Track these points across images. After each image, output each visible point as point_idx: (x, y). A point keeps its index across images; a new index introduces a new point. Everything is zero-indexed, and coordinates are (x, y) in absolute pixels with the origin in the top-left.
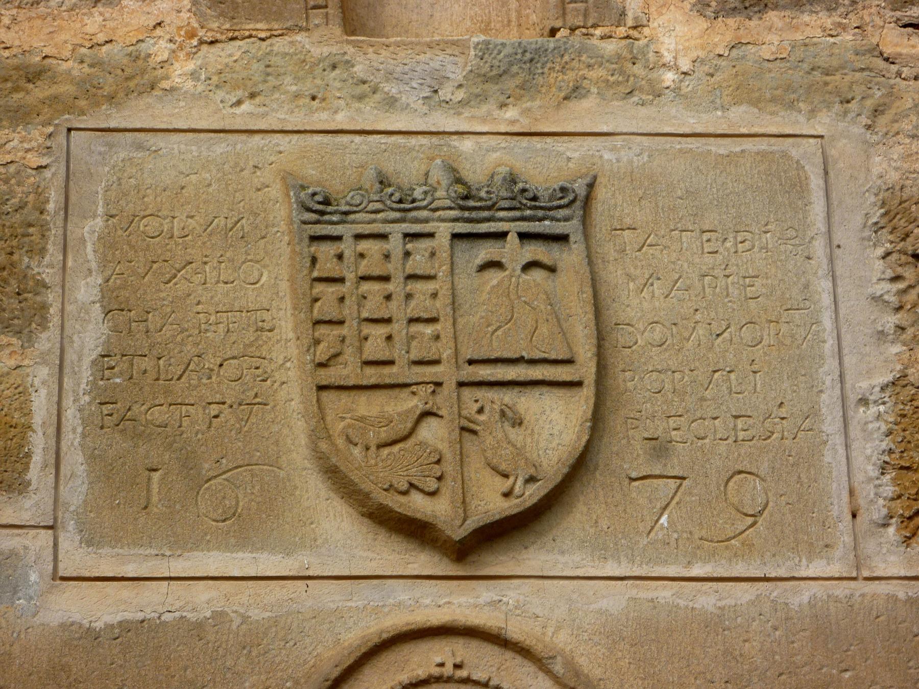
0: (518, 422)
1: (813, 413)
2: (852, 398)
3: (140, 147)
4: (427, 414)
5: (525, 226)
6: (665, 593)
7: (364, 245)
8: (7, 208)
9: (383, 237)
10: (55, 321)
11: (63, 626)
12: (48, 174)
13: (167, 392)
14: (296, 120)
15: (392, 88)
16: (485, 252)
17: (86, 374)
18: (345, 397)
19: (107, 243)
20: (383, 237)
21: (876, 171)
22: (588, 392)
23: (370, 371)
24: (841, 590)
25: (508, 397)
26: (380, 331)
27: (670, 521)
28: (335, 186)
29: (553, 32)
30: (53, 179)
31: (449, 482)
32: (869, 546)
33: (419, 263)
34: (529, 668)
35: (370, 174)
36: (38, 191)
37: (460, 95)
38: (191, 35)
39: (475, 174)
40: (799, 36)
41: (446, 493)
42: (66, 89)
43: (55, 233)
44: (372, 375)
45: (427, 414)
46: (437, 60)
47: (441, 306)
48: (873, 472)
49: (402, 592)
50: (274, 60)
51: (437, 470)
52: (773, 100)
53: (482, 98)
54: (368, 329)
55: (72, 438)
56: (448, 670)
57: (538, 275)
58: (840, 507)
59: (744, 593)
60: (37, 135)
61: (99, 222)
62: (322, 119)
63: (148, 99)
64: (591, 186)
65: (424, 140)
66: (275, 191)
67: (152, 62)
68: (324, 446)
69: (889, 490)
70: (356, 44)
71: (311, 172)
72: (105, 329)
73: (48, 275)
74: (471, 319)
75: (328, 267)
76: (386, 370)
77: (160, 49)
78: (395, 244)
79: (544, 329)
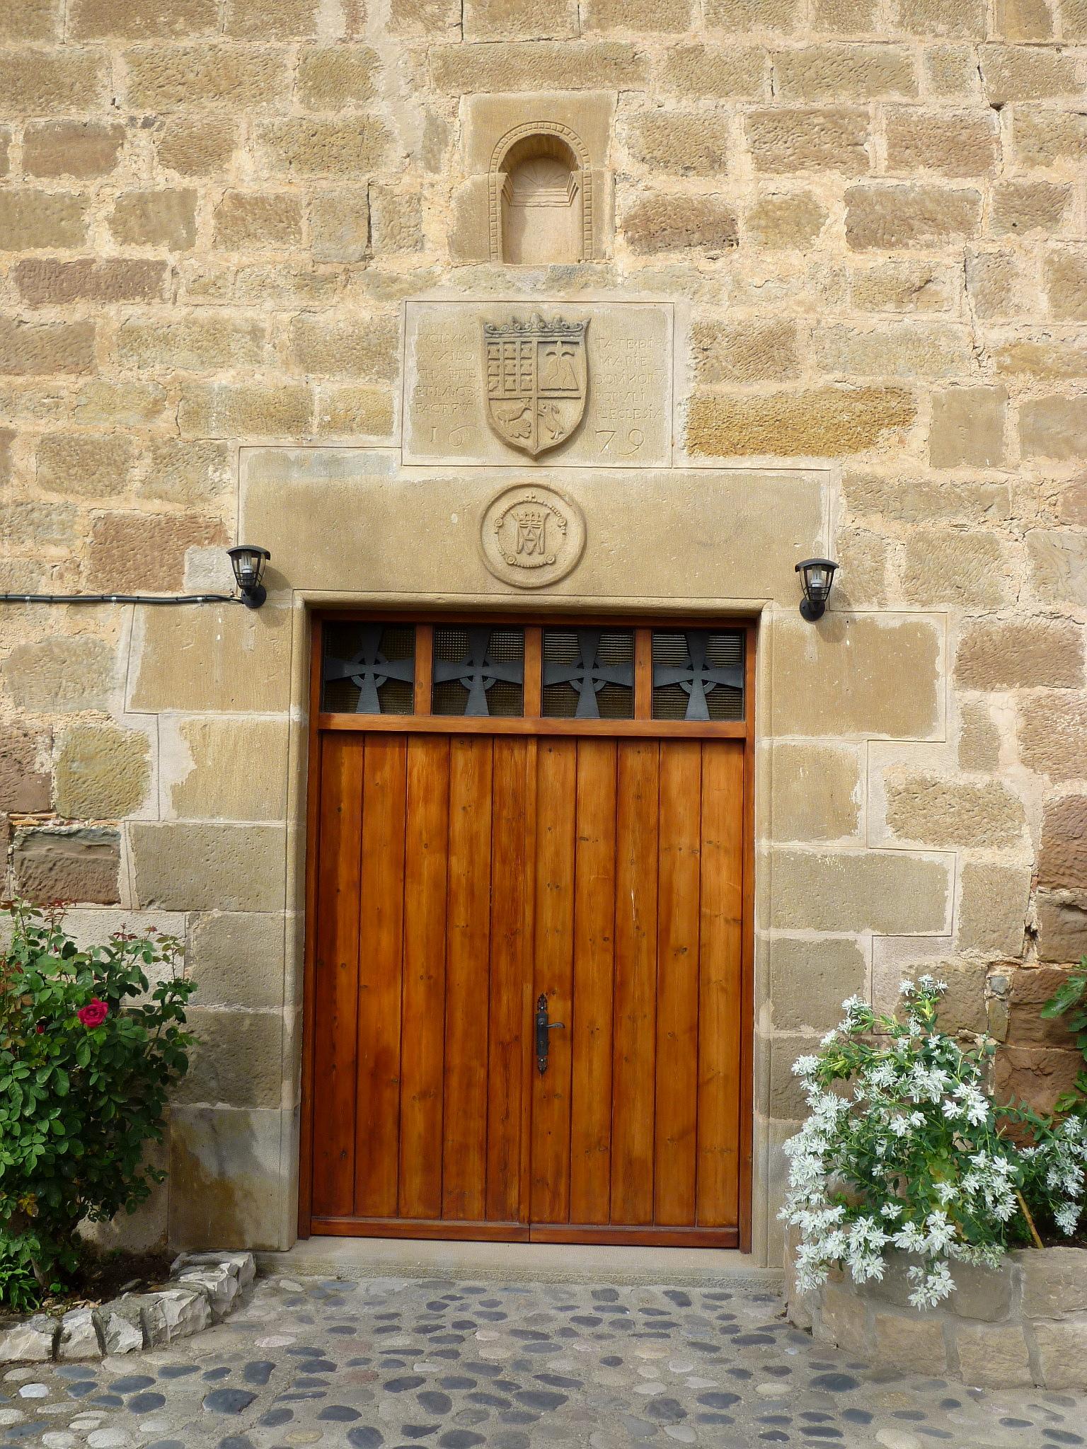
0: (558, 412)
1: (662, 408)
2: (676, 403)
3: (431, 308)
4: (526, 409)
5: (564, 339)
6: (605, 472)
7: (507, 346)
8: (2, 645)
9: (514, 343)
10: (401, 374)
11: (405, 482)
12: (399, 318)
13: (439, 400)
14: (485, 298)
15: (519, 284)
16: (550, 348)
17: (412, 393)
18: (498, 402)
19: (419, 345)
20: (514, 343)
21: (692, 316)
22: (582, 401)
23: (507, 393)
24: (665, 472)
25: (555, 402)
26: (512, 378)
27: (609, 448)
28: (498, 322)
29: (579, 261)
30: (401, 319)
31: (532, 433)
32: (677, 456)
33: (525, 353)
34: (557, 498)
35: (510, 318)
36: (395, 325)
37: (544, 287)
38: (449, 264)
39: (547, 318)
40: (669, 263)
41: (531, 438)
42: (405, 286)
43: (401, 341)
44: (508, 395)
45: (526, 409)
46: (536, 273)
47: (533, 368)
48: (680, 430)
49: (516, 472)
50: (479, 274)
51: (529, 429)
52: (657, 288)
53: (552, 288)
54: (507, 378)
55: (407, 416)
56: (530, 499)
57: (567, 357)
58: (668, 443)
59: (632, 473)
60: (395, 303)
61: (416, 337)
62: (494, 297)
63: (434, 289)
64: (589, 323)
65: (530, 304)
66: (477, 325)
67: (436, 274)
68: (491, 420)
69: (686, 437)
70: (507, 267)
71: (490, 317)
72: (418, 377)
73: (399, 356)
74: (543, 374)
75: (494, 355)
76: (513, 393)
77: (438, 269)
78: (517, 346)
79: (568, 378)
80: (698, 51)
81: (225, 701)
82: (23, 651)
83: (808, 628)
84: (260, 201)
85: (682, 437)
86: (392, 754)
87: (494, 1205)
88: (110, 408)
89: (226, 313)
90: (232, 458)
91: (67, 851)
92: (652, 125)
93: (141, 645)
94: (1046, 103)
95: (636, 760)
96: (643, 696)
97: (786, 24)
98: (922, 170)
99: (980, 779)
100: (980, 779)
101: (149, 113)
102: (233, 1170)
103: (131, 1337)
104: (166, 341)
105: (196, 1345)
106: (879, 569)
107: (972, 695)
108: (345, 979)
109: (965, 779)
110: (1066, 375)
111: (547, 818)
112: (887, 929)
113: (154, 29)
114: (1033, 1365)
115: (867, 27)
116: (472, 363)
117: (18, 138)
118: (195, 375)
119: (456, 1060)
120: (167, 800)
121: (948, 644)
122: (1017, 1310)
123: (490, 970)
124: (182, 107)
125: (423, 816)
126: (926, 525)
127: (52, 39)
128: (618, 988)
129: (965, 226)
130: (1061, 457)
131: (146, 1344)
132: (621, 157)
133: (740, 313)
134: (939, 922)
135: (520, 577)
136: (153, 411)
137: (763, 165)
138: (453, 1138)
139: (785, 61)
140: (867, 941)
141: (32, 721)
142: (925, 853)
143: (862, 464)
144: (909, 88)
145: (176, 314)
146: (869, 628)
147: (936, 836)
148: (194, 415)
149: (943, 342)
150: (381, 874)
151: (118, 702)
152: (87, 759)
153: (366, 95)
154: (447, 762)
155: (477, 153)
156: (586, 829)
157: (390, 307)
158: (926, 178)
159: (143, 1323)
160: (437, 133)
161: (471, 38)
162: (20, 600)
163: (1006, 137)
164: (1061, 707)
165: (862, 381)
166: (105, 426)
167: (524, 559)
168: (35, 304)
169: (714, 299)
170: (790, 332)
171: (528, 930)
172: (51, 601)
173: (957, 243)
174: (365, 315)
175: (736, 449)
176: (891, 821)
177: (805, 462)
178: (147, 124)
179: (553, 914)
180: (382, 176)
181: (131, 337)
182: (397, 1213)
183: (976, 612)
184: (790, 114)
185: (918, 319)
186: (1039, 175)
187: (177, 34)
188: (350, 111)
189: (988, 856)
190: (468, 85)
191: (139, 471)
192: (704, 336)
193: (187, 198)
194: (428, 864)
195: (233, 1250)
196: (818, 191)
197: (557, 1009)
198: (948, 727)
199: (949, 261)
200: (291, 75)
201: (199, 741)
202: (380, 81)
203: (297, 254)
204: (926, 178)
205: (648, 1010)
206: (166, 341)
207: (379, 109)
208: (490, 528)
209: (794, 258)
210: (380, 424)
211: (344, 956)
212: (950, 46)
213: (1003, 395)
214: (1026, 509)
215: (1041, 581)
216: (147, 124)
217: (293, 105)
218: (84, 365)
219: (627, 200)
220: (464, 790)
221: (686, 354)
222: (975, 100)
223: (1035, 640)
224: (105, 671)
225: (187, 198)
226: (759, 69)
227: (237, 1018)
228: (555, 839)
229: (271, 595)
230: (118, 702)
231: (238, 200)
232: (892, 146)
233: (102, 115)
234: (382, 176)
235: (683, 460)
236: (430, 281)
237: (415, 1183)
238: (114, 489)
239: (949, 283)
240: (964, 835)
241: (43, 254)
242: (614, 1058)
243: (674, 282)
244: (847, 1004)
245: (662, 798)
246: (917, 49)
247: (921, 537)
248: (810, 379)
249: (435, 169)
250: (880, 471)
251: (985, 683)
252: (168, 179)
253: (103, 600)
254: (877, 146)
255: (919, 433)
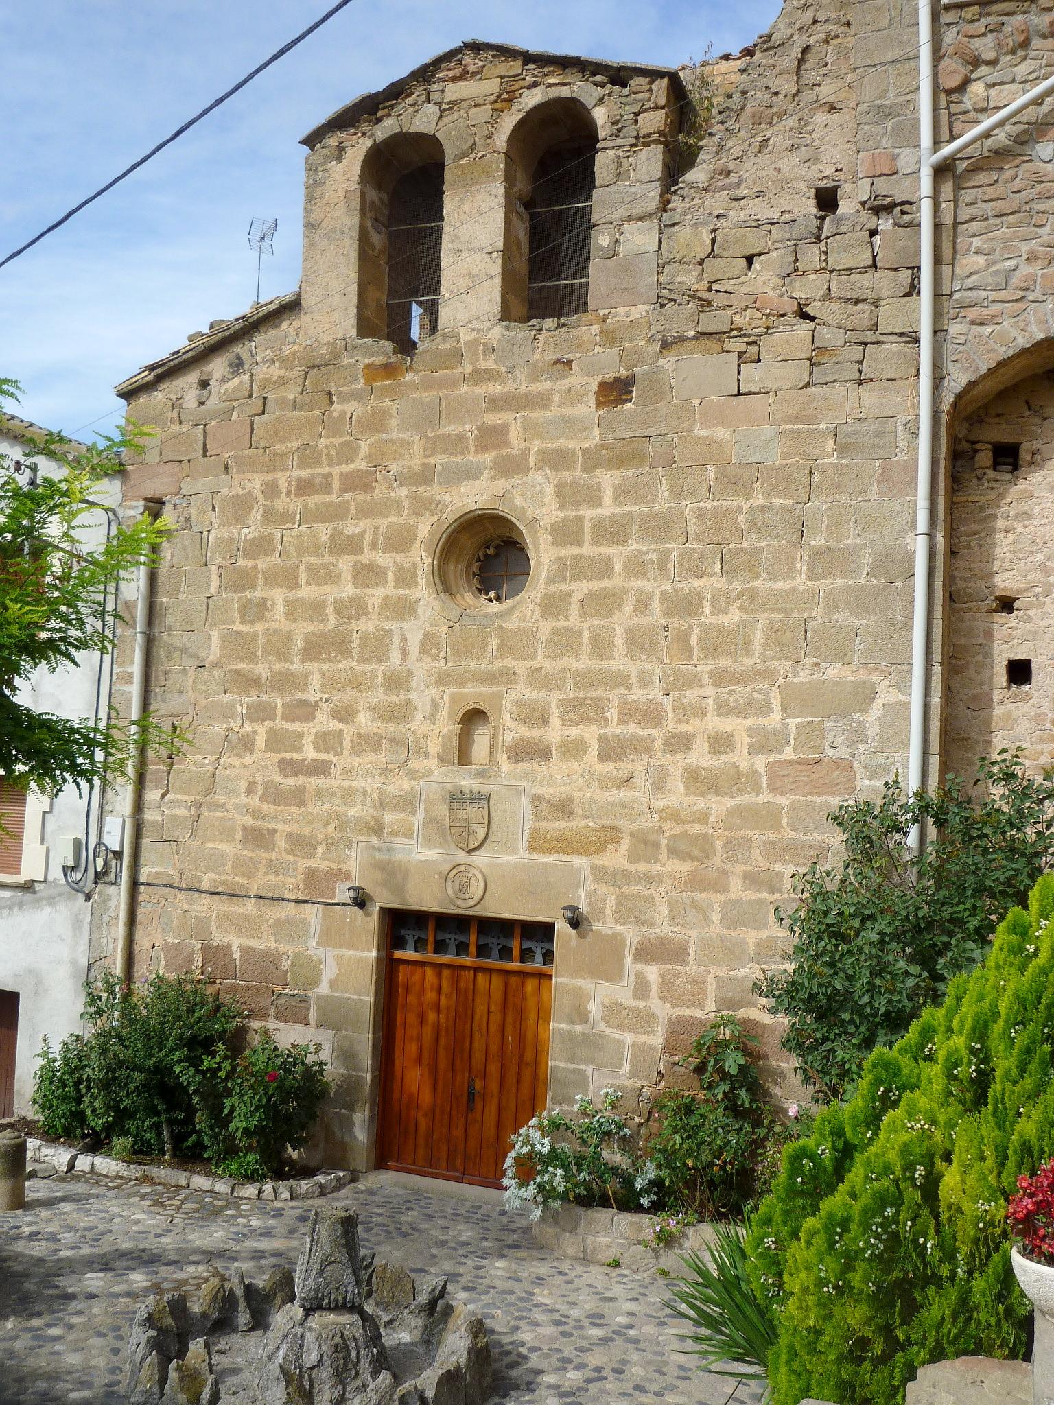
80: (540, 669)
81: (350, 947)
82: (278, 920)
83: (573, 932)
84: (367, 736)
85: (526, 845)
86: (419, 969)
87: (451, 1166)
88: (311, 822)
89: (354, 783)
90: (354, 846)
91: (292, 1002)
92: (520, 703)
93: (320, 921)
94: (688, 693)
95: (513, 980)
96: (516, 953)
97: (577, 656)
98: (632, 725)
99: (641, 1004)
100: (641, 1004)
101: (327, 696)
102: (346, 1138)
103: (286, 1195)
104: (332, 794)
105: (310, 1202)
106: (603, 908)
107: (640, 966)
108: (398, 1062)
109: (634, 1003)
110: (689, 822)
111: (478, 1001)
112: (599, 1066)
113: (329, 659)
114: (584, 1251)
115: (611, 658)
116: (443, 812)
117: (280, 706)
118: (342, 810)
119: (439, 1102)
120: (328, 985)
121: (631, 943)
122: (581, 1230)
123: (453, 1065)
124: (339, 694)
125: (430, 996)
126: (624, 889)
127: (292, 663)
128: (503, 1077)
129: (649, 751)
130: (684, 860)
131: (292, 1198)
132: (507, 719)
133: (552, 791)
134: (620, 1066)
135: (460, 903)
136: (326, 824)
137: (565, 723)
138: (436, 1135)
139: (576, 674)
140: (590, 1070)
141: (281, 949)
142: (617, 1035)
143: (599, 860)
144: (629, 687)
145: (336, 783)
146: (599, 933)
147: (622, 1027)
148: (341, 827)
149: (635, 806)
150: (412, 1018)
151: (312, 943)
152: (300, 966)
153: (408, 689)
154: (439, 975)
155: (450, 717)
156: (493, 1008)
157: (415, 784)
158: (634, 729)
159: (291, 1191)
160: (435, 706)
161: (450, 664)
162: (277, 899)
163: (669, 710)
164: (677, 974)
165: (601, 823)
166: (309, 829)
167: (461, 895)
168: (285, 777)
169: (541, 784)
170: (572, 800)
171: (467, 1050)
172: (288, 900)
173: (645, 759)
174: (405, 787)
175: (548, 851)
176: (603, 1019)
177: (575, 858)
178: (327, 701)
179: (478, 1044)
180: (413, 725)
181: (319, 792)
182: (414, 1164)
183: (644, 929)
184: (577, 699)
185: (626, 795)
186: (683, 727)
187: (339, 661)
188: (402, 697)
189: (643, 1038)
190: (448, 685)
191: (321, 849)
192: (537, 799)
193: (340, 733)
194: (431, 1016)
195: (343, 1170)
196: (586, 735)
197: (478, 1084)
198: (629, 980)
199: (641, 769)
200: (380, 680)
201: (340, 961)
202: (413, 683)
203: (381, 759)
204: (634, 729)
205: (514, 1088)
206: (332, 794)
207: (413, 696)
208: (449, 882)
209: (575, 766)
210: (409, 834)
211: (398, 1053)
212: (646, 666)
213: (661, 830)
214: (667, 884)
215: (672, 917)
216: (327, 701)
217: (380, 694)
218: (302, 804)
219: (509, 738)
220: (445, 985)
221: (529, 808)
222: (656, 692)
223: (669, 943)
224: (307, 930)
225: (340, 733)
226: (565, 678)
227: (350, 1076)
228: (480, 1009)
229: (368, 904)
230: (312, 943)
231: (359, 734)
232: (619, 714)
233: (311, 696)
234: (413, 725)
235: (526, 856)
236: (429, 773)
237: (421, 1151)
238: (312, 856)
239: (640, 779)
240: (633, 1028)
241: (288, 756)
242: (500, 1108)
243: (524, 776)
244: (578, 1097)
245: (523, 997)
246: (632, 668)
247: (622, 894)
248: (578, 822)
249: (434, 723)
250: (607, 864)
251: (646, 962)
252: (334, 725)
253: (306, 902)
254: (613, 714)
255: (624, 847)
